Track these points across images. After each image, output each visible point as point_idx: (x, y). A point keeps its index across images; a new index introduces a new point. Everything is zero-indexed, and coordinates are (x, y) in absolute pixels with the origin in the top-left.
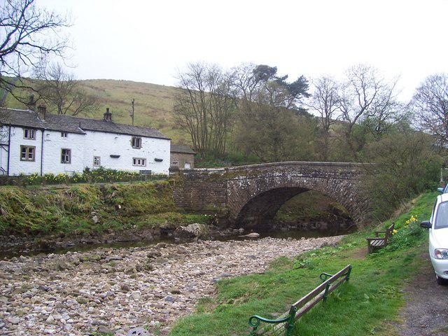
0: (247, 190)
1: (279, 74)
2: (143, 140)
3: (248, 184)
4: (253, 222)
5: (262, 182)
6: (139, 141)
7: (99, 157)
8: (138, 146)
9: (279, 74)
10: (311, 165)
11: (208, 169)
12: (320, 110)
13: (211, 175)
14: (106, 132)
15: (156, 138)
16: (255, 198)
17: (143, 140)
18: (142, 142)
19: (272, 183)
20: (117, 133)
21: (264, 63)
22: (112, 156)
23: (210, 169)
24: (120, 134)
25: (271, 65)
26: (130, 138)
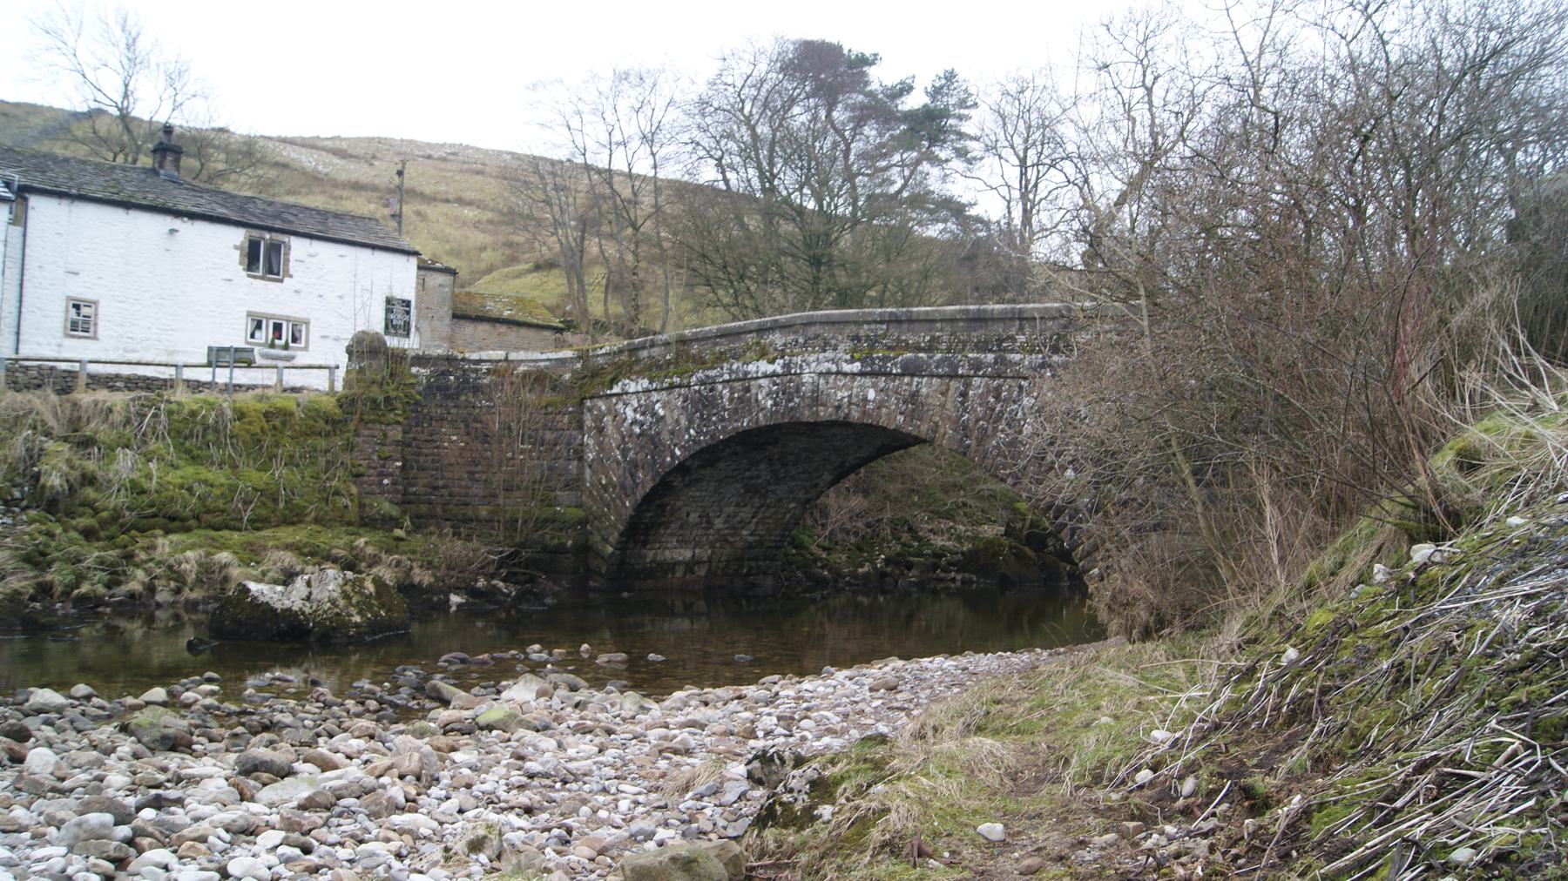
0: (650, 440)
1: (880, 77)
2: (298, 248)
3: (654, 414)
4: (690, 566)
5: (703, 404)
6: (275, 248)
7: (91, 304)
8: (270, 271)
9: (880, 77)
10: (895, 321)
11: (513, 356)
12: (1004, 191)
13: (525, 375)
14: (127, 205)
15: (374, 247)
16: (682, 468)
17: (298, 248)
18: (293, 255)
19: (745, 402)
20: (178, 214)
21: (831, 38)
22: (77, 274)
23: (521, 355)
24: (193, 216)
25: (853, 45)
26: (237, 236)
